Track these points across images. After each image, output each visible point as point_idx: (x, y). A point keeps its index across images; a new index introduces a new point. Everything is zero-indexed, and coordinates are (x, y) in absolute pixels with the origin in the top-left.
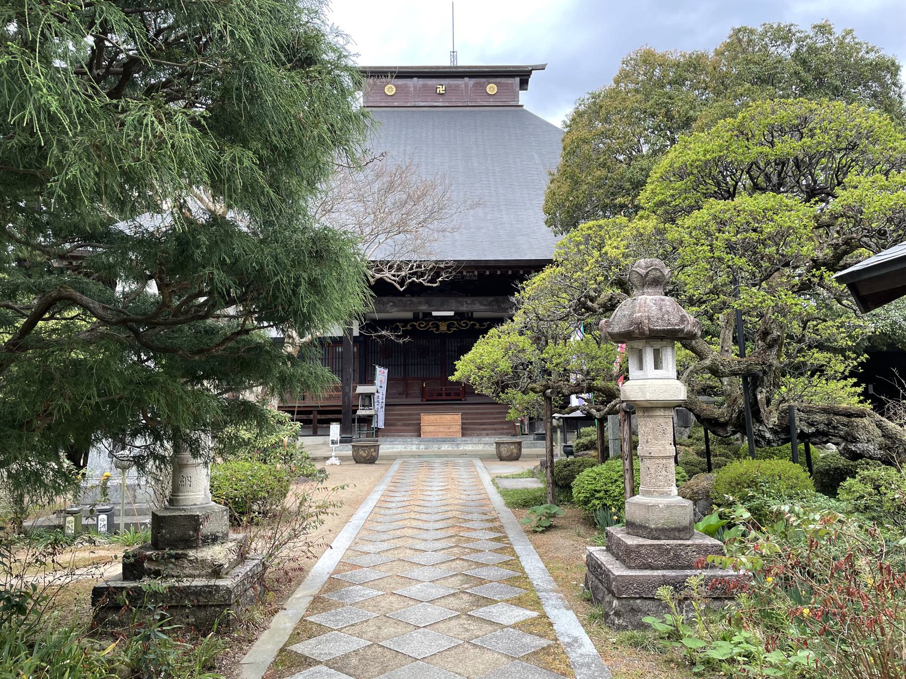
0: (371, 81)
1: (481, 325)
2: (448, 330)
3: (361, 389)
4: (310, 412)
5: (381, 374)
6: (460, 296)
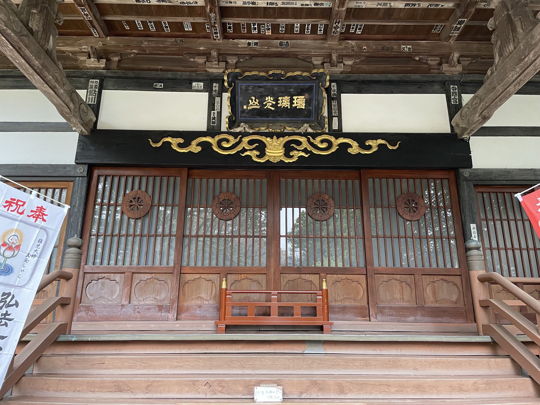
1: (363, 146)
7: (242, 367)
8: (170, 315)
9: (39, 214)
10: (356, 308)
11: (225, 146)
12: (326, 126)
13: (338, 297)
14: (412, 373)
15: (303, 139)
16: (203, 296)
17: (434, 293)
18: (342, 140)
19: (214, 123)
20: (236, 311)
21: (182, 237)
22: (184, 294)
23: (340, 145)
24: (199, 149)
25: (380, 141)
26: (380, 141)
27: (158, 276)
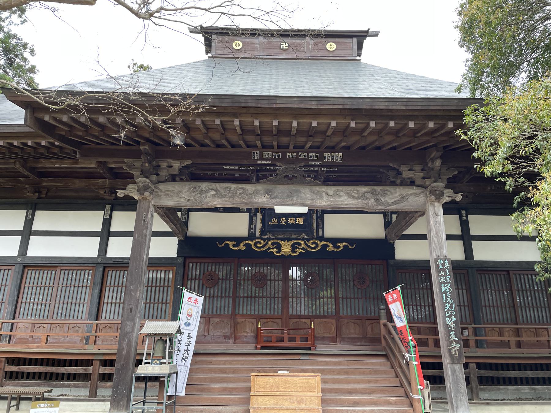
0: (220, 38)
1: (335, 246)
2: (293, 251)
3: (153, 327)
4: (89, 363)
5: (192, 304)
6: (316, 184)
7: (272, 365)
8: (230, 341)
9: (196, 301)
10: (330, 337)
11: (259, 246)
12: (315, 234)
13: (320, 332)
14: (346, 367)
15: (302, 242)
16: (247, 331)
17: (372, 329)
18: (323, 243)
19: (252, 232)
20: (265, 339)
21: (235, 298)
22: (237, 330)
23: (323, 245)
24: (244, 248)
25: (344, 244)
26: (344, 244)
27: (223, 320)
